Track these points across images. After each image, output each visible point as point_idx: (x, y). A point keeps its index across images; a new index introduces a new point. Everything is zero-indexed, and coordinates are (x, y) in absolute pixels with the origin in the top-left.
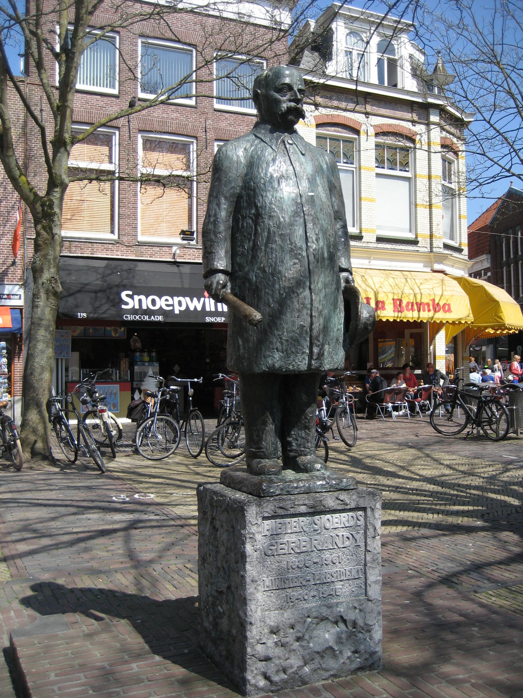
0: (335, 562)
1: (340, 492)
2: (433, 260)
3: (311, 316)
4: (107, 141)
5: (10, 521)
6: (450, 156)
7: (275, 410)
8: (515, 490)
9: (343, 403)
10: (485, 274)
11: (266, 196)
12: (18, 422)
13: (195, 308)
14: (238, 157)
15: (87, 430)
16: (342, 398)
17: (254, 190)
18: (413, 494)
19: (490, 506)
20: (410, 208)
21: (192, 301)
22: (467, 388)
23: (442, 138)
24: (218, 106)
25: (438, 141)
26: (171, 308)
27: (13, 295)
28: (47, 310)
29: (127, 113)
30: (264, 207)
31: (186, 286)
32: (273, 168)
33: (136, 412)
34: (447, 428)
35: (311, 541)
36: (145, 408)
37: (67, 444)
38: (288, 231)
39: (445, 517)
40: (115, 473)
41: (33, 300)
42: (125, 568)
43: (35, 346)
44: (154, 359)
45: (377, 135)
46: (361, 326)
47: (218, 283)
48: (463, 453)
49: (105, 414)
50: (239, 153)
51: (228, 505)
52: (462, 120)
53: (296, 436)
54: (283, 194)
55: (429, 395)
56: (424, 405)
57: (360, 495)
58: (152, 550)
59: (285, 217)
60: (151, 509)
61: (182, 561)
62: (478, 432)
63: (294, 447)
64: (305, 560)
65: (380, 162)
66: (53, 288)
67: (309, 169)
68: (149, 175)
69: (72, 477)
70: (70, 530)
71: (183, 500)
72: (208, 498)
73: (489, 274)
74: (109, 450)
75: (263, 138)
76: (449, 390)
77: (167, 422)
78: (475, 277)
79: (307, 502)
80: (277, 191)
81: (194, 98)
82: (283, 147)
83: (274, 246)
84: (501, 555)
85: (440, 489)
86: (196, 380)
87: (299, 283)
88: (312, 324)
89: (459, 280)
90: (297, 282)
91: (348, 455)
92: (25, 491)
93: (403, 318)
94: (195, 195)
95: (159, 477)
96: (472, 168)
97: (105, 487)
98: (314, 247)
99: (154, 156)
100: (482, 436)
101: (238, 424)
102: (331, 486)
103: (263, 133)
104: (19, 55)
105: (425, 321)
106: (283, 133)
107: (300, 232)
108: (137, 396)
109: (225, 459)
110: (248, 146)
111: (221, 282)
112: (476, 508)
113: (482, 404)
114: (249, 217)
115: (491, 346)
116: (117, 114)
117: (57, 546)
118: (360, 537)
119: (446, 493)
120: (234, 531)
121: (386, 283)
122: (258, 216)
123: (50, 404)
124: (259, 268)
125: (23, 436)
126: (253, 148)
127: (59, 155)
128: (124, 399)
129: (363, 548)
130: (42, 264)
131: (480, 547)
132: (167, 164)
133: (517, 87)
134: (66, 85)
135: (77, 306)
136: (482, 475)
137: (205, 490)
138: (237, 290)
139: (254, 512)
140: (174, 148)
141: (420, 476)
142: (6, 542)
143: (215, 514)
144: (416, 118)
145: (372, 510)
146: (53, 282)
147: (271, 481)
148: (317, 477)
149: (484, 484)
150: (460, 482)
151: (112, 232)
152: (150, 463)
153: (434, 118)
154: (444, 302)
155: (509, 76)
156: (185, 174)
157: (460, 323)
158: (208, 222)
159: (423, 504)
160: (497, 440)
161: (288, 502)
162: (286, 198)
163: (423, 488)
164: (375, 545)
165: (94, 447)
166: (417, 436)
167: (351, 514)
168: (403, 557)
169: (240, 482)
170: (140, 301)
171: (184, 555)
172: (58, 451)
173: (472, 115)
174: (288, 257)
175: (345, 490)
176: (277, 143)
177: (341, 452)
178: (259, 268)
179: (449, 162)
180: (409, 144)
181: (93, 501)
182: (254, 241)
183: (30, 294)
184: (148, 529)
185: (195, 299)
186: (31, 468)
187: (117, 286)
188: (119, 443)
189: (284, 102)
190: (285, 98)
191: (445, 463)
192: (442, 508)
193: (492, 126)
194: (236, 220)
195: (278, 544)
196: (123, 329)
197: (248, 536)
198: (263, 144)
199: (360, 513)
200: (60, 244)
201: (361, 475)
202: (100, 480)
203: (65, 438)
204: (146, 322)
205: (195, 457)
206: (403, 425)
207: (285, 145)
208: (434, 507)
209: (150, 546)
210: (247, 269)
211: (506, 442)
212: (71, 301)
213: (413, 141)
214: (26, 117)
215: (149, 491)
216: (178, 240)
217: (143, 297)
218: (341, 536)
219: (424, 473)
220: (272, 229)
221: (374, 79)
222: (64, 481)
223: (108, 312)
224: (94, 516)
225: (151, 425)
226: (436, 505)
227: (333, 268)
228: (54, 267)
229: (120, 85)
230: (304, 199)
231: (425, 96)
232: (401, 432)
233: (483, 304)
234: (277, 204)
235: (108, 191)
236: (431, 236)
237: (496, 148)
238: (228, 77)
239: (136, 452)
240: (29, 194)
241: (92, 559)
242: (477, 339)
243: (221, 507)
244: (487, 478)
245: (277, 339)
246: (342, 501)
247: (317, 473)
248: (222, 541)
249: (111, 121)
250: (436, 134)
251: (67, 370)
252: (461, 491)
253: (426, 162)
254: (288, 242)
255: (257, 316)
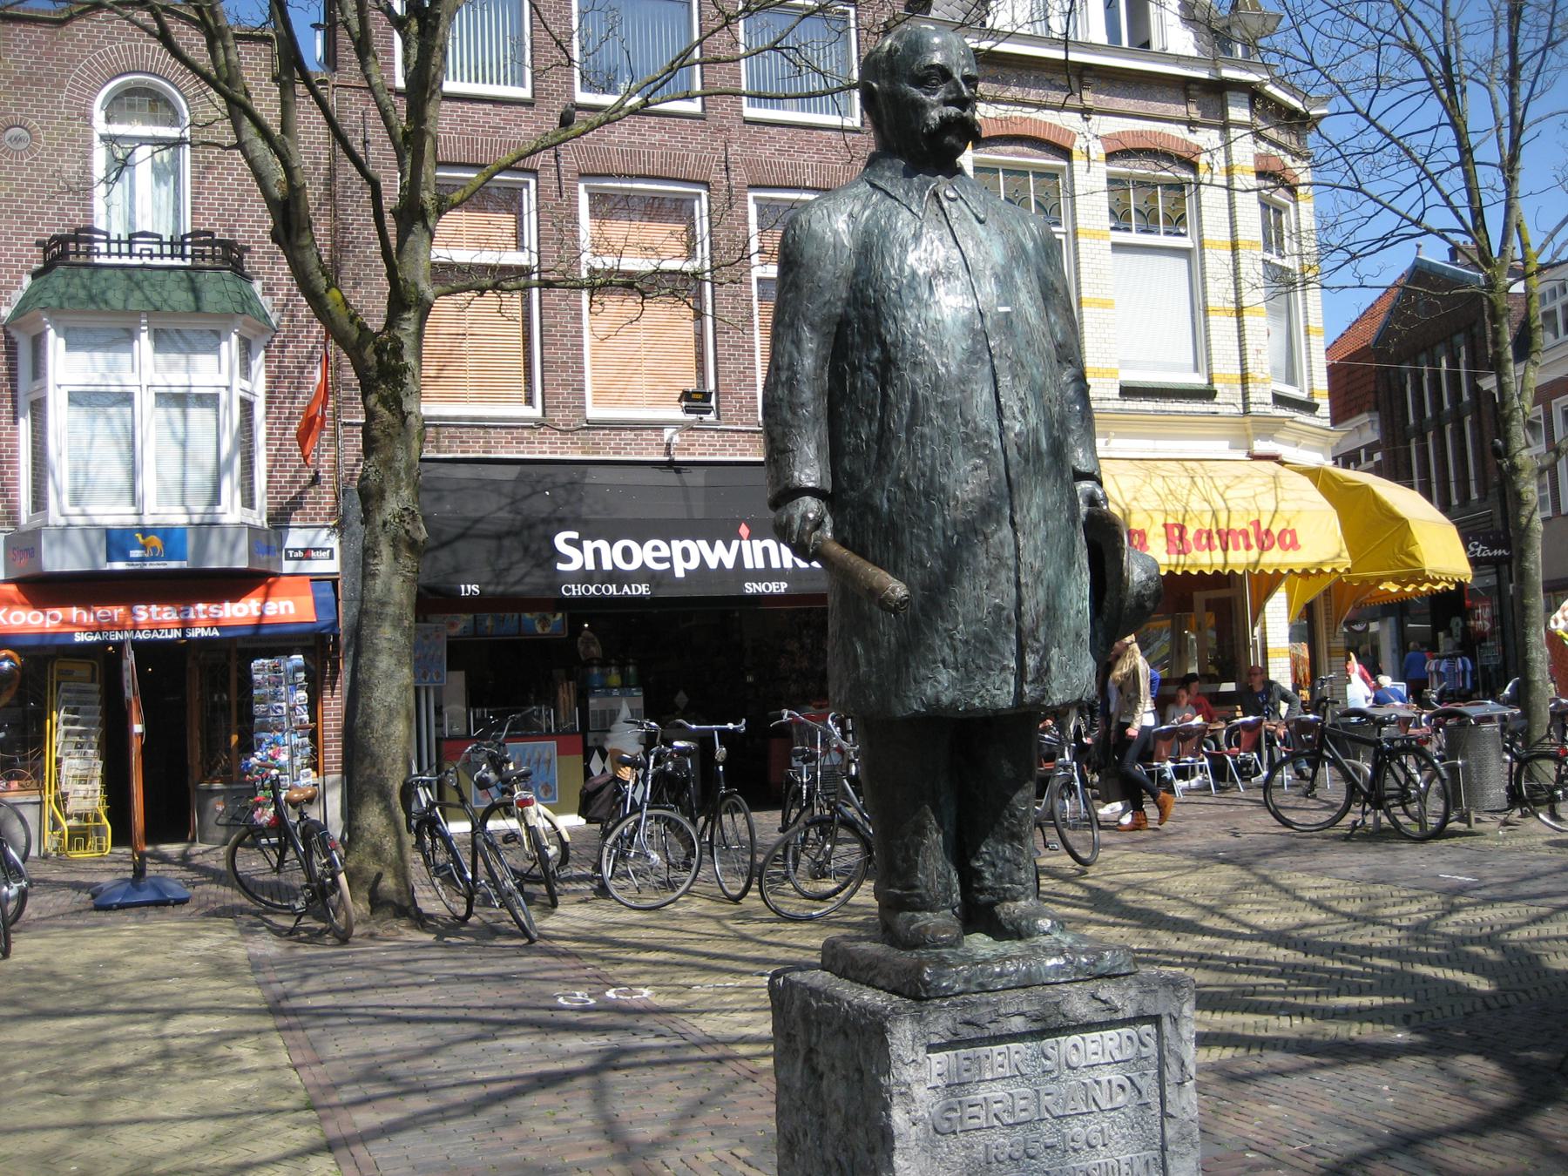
0: (1093, 1142)
1: (1099, 982)
2: (1250, 431)
3: (1018, 585)
4: (511, 201)
5: (334, 1059)
6: (1281, 196)
7: (942, 800)
8: (1478, 956)
9: (1065, 767)
10: (1369, 457)
11: (904, 320)
12: (336, 829)
13: (721, 562)
14: (836, 233)
15: (493, 847)
16: (1063, 756)
17: (876, 307)
18: (1240, 971)
19: (1421, 994)
20: (1193, 318)
21: (712, 547)
22: (1344, 720)
23: (1258, 157)
24: (750, 112)
25: (1250, 164)
26: (666, 566)
27: (316, 550)
28: (397, 583)
29: (556, 140)
30: (900, 344)
31: (699, 514)
32: (920, 253)
33: (598, 802)
34: (1304, 813)
35: (1038, 1098)
36: (619, 792)
37: (449, 880)
38: (958, 396)
39: (1318, 1022)
40: (558, 943)
41: (363, 561)
42: (600, 1161)
43: (372, 664)
44: (633, 681)
45: (1110, 156)
46: (1130, 602)
47: (804, 518)
48: (1346, 871)
49: (532, 810)
50: (837, 225)
51: (846, 1019)
52: (1306, 116)
53: (990, 856)
54: (941, 313)
55: (1256, 738)
56: (1247, 763)
57: (1146, 987)
58: (656, 1119)
59: (948, 363)
60: (645, 1022)
61: (727, 1142)
62: (1377, 821)
63: (989, 881)
64: (1026, 1141)
65: (1120, 218)
66: (407, 532)
67: (997, 253)
68: (610, 272)
69: (463, 954)
70: (469, 1075)
71: (717, 1000)
72: (797, 1003)
73: (1378, 457)
74: (543, 888)
75: (889, 189)
76: (1303, 726)
77: (669, 822)
78: (1346, 466)
79: (1025, 1008)
80: (927, 306)
81: (699, 100)
82: (936, 207)
83: (927, 430)
84: (1460, 1111)
85: (1300, 957)
86: (731, 726)
87: (989, 510)
88: (1020, 601)
89: (1314, 474)
90: (983, 509)
91: (1081, 885)
92: (363, 988)
93: (1191, 566)
94: (709, 311)
95: (658, 949)
96: (1332, 220)
97: (538, 975)
98: (1017, 429)
99: (618, 229)
100: (1387, 830)
101: (832, 821)
102: (1079, 969)
103: (889, 177)
104: (314, 26)
105: (1240, 572)
106: (934, 175)
107: (984, 395)
108: (596, 765)
109: (804, 901)
110: (856, 209)
111: (811, 516)
112: (1389, 1000)
113: (1384, 758)
114: (868, 367)
115: (1391, 620)
116: (534, 143)
117: (442, 1114)
118: (1148, 1084)
119: (1316, 968)
120: (861, 1080)
121: (1147, 489)
122: (888, 364)
123: (408, 793)
124: (896, 482)
125: (351, 865)
126: (867, 213)
127: (411, 238)
128: (567, 772)
129: (1157, 1110)
130: (382, 481)
131: (1408, 1093)
132: (646, 247)
133: (1427, 33)
134: (422, 84)
135: (457, 570)
136: (1396, 921)
137: (790, 985)
138: (847, 532)
139: (908, 1034)
140: (655, 208)
141: (1252, 927)
142: (330, 1107)
143: (814, 1039)
144: (1196, 114)
145: (1175, 1021)
146: (407, 519)
147: (942, 963)
148: (1044, 949)
149: (1404, 943)
150: (1347, 940)
151: (529, 401)
152: (636, 915)
153: (1238, 112)
154: (1283, 525)
155: (1407, 11)
156: (688, 267)
157: (1320, 572)
158: (776, 383)
159: (1265, 993)
160: (1423, 838)
161: (983, 1010)
162: (948, 320)
163: (1263, 957)
164: (1187, 1102)
165: (509, 884)
166: (1235, 835)
167: (1125, 1031)
168: (1231, 1120)
169: (870, 967)
170: (597, 552)
171: (728, 1127)
172: (428, 895)
173: (1326, 100)
174: (959, 453)
175: (1109, 977)
176: (921, 198)
177: (1066, 879)
178: (896, 482)
179: (1275, 210)
180: (1186, 175)
181: (514, 1008)
182: (881, 420)
183: (357, 547)
184: (644, 1070)
185: (719, 544)
186: (372, 936)
187: (546, 521)
188: (563, 874)
189: (933, 107)
190: (934, 98)
191: (1308, 895)
192: (1311, 1001)
193: (1373, 123)
194: (837, 376)
195: (965, 1106)
196: (559, 616)
197: (895, 1090)
198: (889, 201)
199: (1148, 1028)
200: (420, 434)
201: (1116, 931)
202: (526, 960)
203: (444, 867)
204: (612, 599)
205: (736, 900)
206: (1202, 810)
207: (939, 202)
208: (1291, 1000)
209: (651, 1107)
210: (867, 484)
211: (1444, 842)
212: (445, 558)
213: (1193, 166)
214: (333, 156)
215: (637, 981)
216: (677, 413)
217: (602, 544)
218: (1105, 1083)
219: (1261, 920)
220: (920, 392)
221: (1099, 35)
222: (448, 964)
223: (527, 580)
224: (521, 1042)
225: (634, 831)
226: (1295, 995)
227: (1060, 473)
228: (408, 486)
229: (534, 79)
230: (988, 322)
231: (1214, 65)
232: (1199, 826)
233: (1372, 527)
234: (929, 336)
235: (518, 312)
236: (1244, 378)
237: (1384, 173)
238: (775, 49)
239: (603, 891)
240: (348, 327)
241: (522, 1142)
242: (1358, 608)
243: (829, 1025)
244: (1407, 928)
245: (943, 640)
246: (1105, 1002)
247: (1044, 940)
248: (835, 1102)
249: (522, 157)
250: (1245, 150)
251: (439, 711)
252: (1351, 962)
253: (1225, 212)
254: (959, 420)
255: (899, 589)
